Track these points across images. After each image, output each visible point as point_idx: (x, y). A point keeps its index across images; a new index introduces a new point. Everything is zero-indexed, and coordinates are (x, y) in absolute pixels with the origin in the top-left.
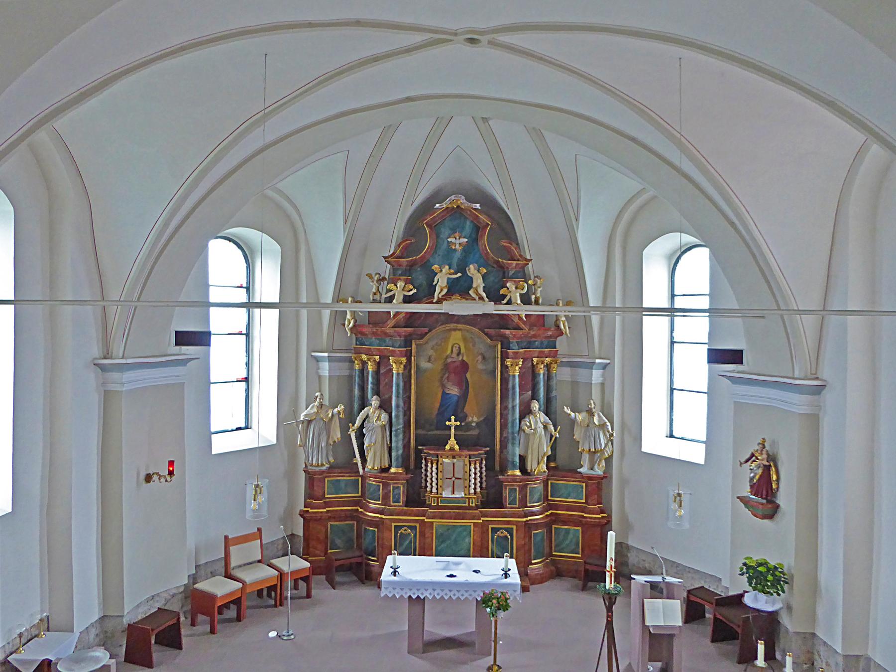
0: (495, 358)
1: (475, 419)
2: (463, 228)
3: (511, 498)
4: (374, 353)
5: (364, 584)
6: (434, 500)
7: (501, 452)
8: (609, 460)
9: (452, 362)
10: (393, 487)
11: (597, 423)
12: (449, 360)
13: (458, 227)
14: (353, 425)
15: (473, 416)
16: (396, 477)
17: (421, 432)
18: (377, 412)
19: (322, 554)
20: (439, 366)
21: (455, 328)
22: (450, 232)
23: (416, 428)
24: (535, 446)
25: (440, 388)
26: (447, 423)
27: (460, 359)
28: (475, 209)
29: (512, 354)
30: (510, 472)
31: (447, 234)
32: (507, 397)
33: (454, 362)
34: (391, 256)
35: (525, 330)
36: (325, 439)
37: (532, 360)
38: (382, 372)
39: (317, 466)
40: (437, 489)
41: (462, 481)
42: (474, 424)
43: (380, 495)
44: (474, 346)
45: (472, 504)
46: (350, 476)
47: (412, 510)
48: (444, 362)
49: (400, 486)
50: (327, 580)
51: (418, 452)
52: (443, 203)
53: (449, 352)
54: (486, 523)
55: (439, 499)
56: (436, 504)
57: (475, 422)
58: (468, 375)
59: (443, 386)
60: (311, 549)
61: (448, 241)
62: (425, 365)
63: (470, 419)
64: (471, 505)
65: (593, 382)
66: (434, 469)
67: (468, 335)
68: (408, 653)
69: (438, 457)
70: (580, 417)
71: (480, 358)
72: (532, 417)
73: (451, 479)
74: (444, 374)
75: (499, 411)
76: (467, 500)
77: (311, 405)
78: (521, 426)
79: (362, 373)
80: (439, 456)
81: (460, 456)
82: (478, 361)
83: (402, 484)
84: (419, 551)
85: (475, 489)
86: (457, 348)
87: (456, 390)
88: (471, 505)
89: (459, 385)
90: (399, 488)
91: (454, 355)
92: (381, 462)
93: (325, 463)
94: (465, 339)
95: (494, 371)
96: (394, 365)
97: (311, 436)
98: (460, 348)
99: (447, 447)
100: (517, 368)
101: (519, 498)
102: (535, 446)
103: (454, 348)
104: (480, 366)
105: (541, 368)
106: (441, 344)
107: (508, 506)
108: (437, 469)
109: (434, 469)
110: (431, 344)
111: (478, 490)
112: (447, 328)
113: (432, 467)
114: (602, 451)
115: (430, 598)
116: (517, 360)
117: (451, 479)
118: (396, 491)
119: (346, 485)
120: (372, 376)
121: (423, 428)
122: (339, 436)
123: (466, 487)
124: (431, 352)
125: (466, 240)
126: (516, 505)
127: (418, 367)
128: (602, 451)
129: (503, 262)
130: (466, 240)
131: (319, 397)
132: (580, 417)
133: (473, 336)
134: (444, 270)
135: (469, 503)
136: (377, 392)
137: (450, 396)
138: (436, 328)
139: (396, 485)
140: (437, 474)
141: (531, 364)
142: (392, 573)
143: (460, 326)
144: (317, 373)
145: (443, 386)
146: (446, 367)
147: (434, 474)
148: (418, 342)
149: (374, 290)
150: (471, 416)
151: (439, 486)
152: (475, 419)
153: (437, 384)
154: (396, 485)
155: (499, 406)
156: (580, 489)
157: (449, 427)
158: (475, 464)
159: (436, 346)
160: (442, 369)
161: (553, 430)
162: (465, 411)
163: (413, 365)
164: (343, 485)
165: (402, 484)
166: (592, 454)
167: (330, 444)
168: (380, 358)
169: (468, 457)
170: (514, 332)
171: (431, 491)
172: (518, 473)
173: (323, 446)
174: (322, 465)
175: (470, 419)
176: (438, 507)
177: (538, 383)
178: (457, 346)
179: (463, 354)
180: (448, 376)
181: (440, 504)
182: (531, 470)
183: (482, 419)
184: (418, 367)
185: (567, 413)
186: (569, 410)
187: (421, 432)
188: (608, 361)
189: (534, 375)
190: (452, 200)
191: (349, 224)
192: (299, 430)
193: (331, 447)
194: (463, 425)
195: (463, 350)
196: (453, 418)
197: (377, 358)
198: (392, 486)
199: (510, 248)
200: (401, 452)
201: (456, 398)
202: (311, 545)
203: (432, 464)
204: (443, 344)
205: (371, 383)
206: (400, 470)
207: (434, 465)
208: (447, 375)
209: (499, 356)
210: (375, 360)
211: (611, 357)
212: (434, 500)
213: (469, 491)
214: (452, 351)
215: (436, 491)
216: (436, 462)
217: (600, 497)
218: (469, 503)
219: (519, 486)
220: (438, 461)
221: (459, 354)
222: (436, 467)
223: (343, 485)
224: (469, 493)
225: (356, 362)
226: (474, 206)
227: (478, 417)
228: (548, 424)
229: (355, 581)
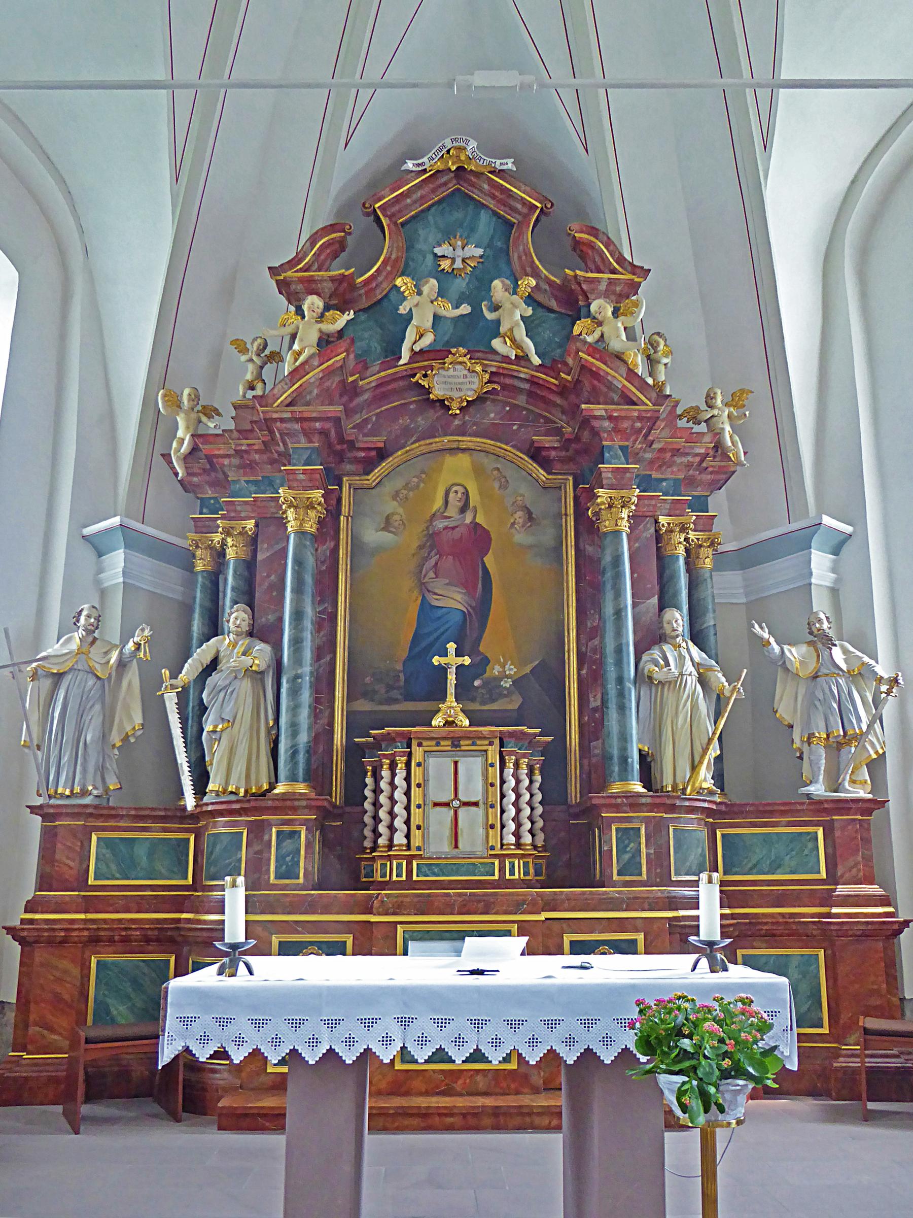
0: (560, 516)
1: (511, 670)
2: (472, 229)
3: (626, 857)
4: (243, 515)
5: (178, 1120)
6: (399, 866)
7: (584, 749)
8: (876, 766)
9: (446, 528)
10: (278, 833)
11: (844, 667)
12: (440, 524)
13: (461, 225)
14: (174, 676)
15: (505, 663)
16: (287, 804)
17: (363, 705)
18: (244, 643)
19: (66, 1044)
20: (412, 538)
21: (455, 445)
22: (440, 236)
23: (351, 697)
24: (682, 719)
25: (416, 593)
26: (436, 660)
27: (468, 521)
28: (500, 173)
29: (610, 475)
30: (616, 788)
31: (431, 239)
32: (598, 588)
33: (453, 528)
34: (292, 263)
35: (647, 405)
36: (97, 721)
37: (656, 522)
38: (260, 557)
39: (68, 797)
40: (408, 836)
41: (479, 812)
42: (507, 684)
43: (240, 860)
44: (504, 486)
45: (512, 873)
46: (165, 830)
47: (335, 896)
48: (427, 528)
49: (297, 828)
50: (65, 1114)
51: (354, 752)
52: (425, 159)
53: (439, 503)
54: (556, 926)
55: (415, 863)
56: (404, 878)
57: (508, 677)
58: (489, 560)
59: (423, 587)
60: (33, 1030)
61: (435, 255)
62: (372, 536)
63: (497, 670)
64: (508, 877)
65: (813, 581)
66: (399, 780)
67: (488, 463)
68: (489, 662)
69: (409, 746)
70: (794, 654)
71: (519, 516)
72: (666, 648)
73: (447, 804)
74: (426, 559)
75: (573, 646)
76: (497, 862)
77: (66, 637)
78: (641, 665)
79: (211, 581)
80: (414, 743)
81: (475, 738)
82: (513, 524)
83: (304, 823)
84: (325, 237)
85: (517, 834)
86: (459, 495)
87: (459, 597)
88: (508, 877)
89: (468, 586)
90: (295, 834)
91: (452, 511)
92: (248, 776)
93: (90, 788)
94: (478, 472)
95: (557, 551)
96: (291, 514)
97: (57, 714)
98: (466, 493)
99: (438, 721)
100: (625, 514)
101: (648, 855)
102: (682, 719)
103: (452, 495)
104: (521, 538)
105: (680, 543)
106: (418, 486)
107: (615, 877)
108: (408, 779)
109: (399, 780)
110: (389, 488)
111: (527, 839)
112: (434, 447)
113: (393, 775)
114: (860, 738)
115: (827, 1032)
116: (623, 492)
117: (447, 804)
118: (288, 844)
119: (151, 854)
120: (235, 571)
121: (367, 695)
122: (138, 719)
123: (492, 827)
124: (391, 506)
125: (480, 251)
126: (640, 874)
127: (357, 546)
128: (860, 738)
129: (576, 276)
130: (480, 251)
131: (85, 613)
132: (794, 654)
133: (499, 466)
134: (426, 289)
135: (502, 869)
136: (247, 596)
137: (440, 613)
138: (405, 447)
139: (286, 828)
140: (408, 793)
141: (652, 530)
142: (222, 1047)
143: (467, 441)
144: (97, 582)
145: (423, 587)
146: (432, 541)
147: (399, 795)
148: (357, 480)
149: (249, 377)
150: (498, 662)
151: (413, 827)
152: (511, 670)
153: (408, 583)
154: (286, 828)
155: (573, 634)
156: (810, 845)
157: (443, 670)
158: (517, 765)
159: (405, 492)
160: (421, 547)
161: (726, 684)
162: (481, 649)
163: (342, 536)
164: (141, 852)
165: (304, 823)
166: (836, 746)
167: (114, 746)
168: (257, 525)
169: (497, 741)
170: (617, 410)
171: (390, 846)
172: (638, 788)
173: (89, 738)
174: (84, 793)
175: (497, 670)
176: (410, 884)
177: (674, 577)
178: (460, 490)
179: (475, 507)
180: (436, 564)
181: (415, 878)
182: (675, 787)
183: (527, 670)
184: (357, 546)
185: (762, 639)
186: (767, 630)
187: (363, 705)
188: (848, 529)
189: (663, 562)
190: (444, 151)
191: (183, 178)
192: (24, 706)
193: (116, 751)
194: (477, 688)
195: (475, 498)
196: (452, 647)
197: (250, 524)
198: (274, 830)
199: (591, 246)
200: (303, 738)
201: (457, 618)
202: (33, 1017)
203: (393, 767)
204: (422, 485)
205: (233, 589)
206: (302, 788)
207: (401, 774)
208: (433, 561)
209: (571, 510)
210: (243, 533)
211: (856, 516)
212: (399, 866)
213: (502, 839)
214: (446, 502)
215: (405, 841)
216: (404, 759)
217: (868, 859)
218: (502, 869)
219: (647, 821)
220: (410, 755)
221: (463, 510)
222: (404, 774)
223: (141, 852)
224: (502, 845)
225: (199, 553)
226: (498, 164)
227: (520, 664)
228: (710, 669)
229: (155, 1116)
